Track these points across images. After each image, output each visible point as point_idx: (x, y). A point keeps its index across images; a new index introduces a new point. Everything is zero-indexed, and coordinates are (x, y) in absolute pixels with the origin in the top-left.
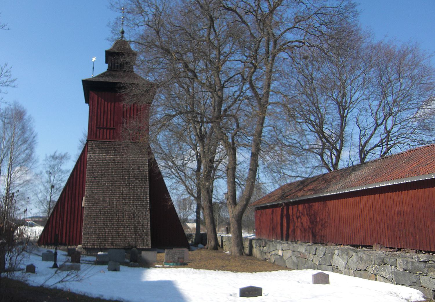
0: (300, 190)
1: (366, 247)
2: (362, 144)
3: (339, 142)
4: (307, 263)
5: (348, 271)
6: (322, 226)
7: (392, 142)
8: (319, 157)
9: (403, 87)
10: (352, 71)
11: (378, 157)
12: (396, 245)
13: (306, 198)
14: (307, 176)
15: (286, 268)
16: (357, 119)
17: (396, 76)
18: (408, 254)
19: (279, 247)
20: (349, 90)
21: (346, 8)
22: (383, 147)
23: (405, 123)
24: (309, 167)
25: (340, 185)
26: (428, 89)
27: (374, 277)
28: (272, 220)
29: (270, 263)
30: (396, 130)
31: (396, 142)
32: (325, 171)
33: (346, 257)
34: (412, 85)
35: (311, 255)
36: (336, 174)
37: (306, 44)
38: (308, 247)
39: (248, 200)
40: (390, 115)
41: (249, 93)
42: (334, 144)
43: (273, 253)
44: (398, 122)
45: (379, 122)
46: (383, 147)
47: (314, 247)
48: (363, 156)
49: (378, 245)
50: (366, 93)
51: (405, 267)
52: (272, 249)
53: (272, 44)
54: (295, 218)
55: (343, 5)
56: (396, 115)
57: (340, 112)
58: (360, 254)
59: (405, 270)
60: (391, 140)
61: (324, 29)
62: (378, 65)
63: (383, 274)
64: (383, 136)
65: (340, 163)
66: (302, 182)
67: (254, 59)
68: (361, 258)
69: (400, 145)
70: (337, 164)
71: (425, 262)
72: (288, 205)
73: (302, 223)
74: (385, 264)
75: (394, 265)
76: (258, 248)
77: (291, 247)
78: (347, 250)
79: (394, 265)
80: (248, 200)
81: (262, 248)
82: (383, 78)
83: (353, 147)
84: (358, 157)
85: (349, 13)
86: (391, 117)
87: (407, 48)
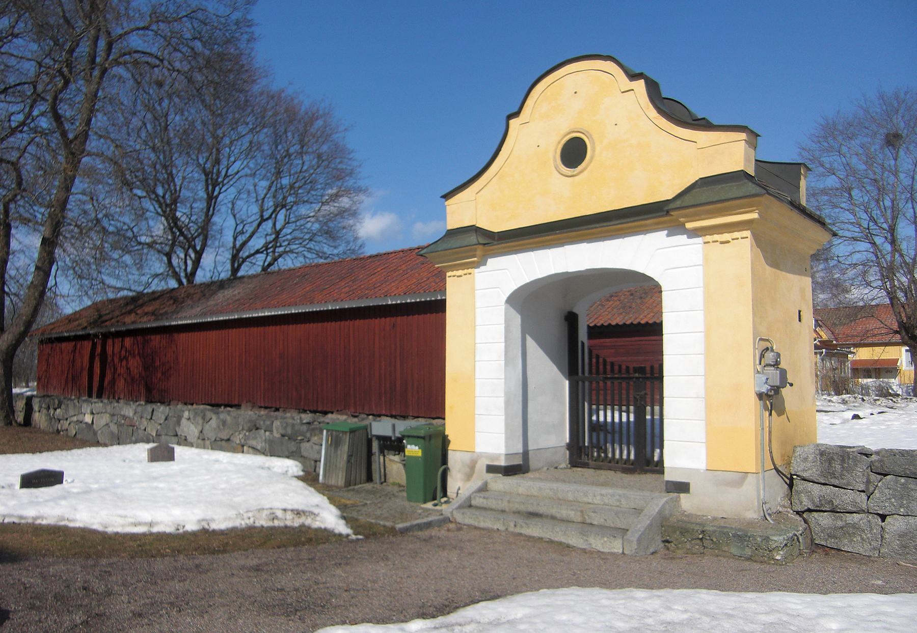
0: (130, 312)
1: (231, 406)
2: (238, 246)
3: (201, 237)
4: (135, 434)
5: (203, 442)
6: (163, 374)
7: (281, 249)
8: (165, 259)
9: (305, 168)
10: (235, 124)
11: (259, 269)
12: (273, 404)
13: (140, 326)
14: (141, 289)
15: (97, 444)
16: (233, 204)
17: (297, 147)
18: (288, 415)
19: (86, 408)
20: (226, 155)
21: (237, 23)
22: (267, 254)
23: (302, 222)
24: (149, 275)
25: (199, 309)
26: (338, 178)
27: (240, 448)
28: (74, 361)
29: (67, 436)
30: (289, 231)
31: (288, 249)
32: (173, 284)
33: (200, 421)
34: (318, 167)
35: (144, 420)
36: (189, 291)
37: (166, 63)
38: (139, 409)
39: (29, 324)
40: (284, 206)
41: (44, 123)
42: (189, 239)
43: (75, 419)
44: (293, 219)
45: (266, 215)
46: (267, 254)
47: (149, 408)
48: (236, 265)
49: (248, 404)
50: (252, 165)
51: (283, 432)
52: (71, 412)
53: (102, 44)
54: (116, 360)
55: (234, 17)
56: (291, 209)
57: (207, 188)
58: (222, 416)
59: (283, 436)
60: (281, 246)
61: (198, 45)
62: (274, 125)
63: (253, 443)
64: (270, 238)
65: (199, 273)
66: (134, 300)
67: (67, 66)
68: (224, 423)
69: (293, 256)
70: (193, 273)
71: (309, 423)
72: (106, 336)
73: (128, 369)
74: (257, 429)
75: (269, 429)
76: (44, 411)
77: (109, 408)
78: (202, 411)
79: (269, 429)
80: (29, 324)
81: (52, 411)
82: (280, 147)
83: (222, 249)
84: (228, 266)
85: (242, 34)
86: (284, 211)
87: (318, 110)
